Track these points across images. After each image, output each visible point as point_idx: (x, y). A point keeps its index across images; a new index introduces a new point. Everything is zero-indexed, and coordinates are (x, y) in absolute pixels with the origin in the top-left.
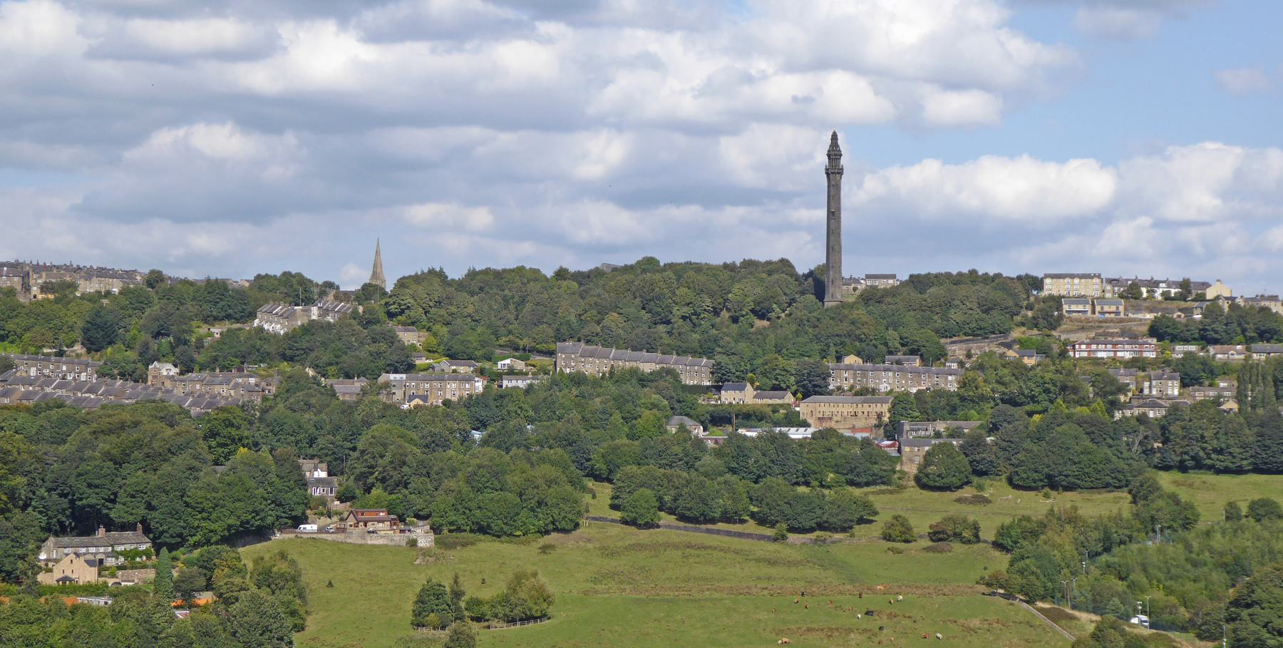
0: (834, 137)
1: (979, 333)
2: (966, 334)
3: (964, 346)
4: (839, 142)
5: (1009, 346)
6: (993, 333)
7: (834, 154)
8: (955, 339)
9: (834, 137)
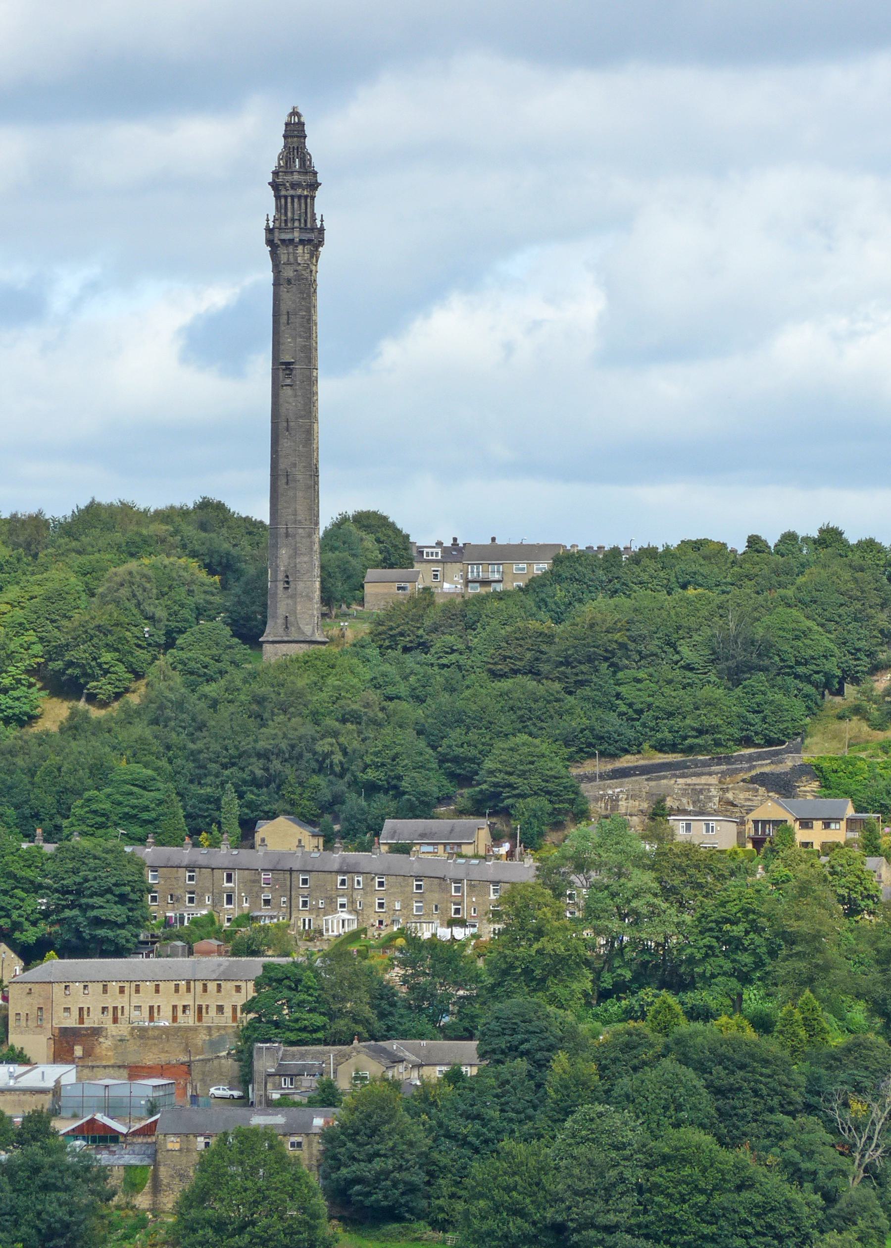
0: (295, 132)
1: (691, 744)
2: (661, 747)
3: (643, 784)
4: (311, 144)
5: (783, 786)
6: (747, 742)
7: (295, 180)
8: (627, 761)
9: (295, 132)
